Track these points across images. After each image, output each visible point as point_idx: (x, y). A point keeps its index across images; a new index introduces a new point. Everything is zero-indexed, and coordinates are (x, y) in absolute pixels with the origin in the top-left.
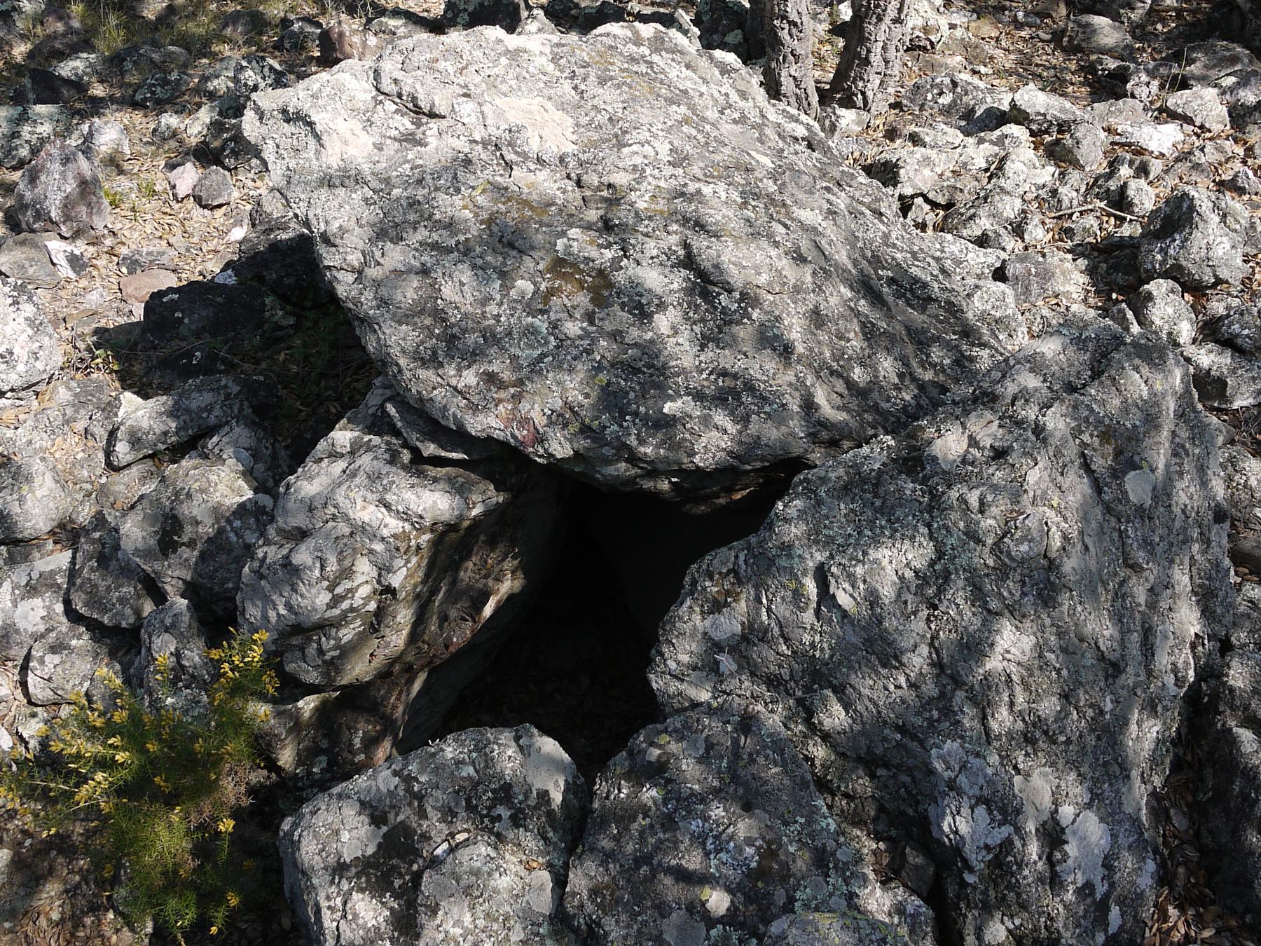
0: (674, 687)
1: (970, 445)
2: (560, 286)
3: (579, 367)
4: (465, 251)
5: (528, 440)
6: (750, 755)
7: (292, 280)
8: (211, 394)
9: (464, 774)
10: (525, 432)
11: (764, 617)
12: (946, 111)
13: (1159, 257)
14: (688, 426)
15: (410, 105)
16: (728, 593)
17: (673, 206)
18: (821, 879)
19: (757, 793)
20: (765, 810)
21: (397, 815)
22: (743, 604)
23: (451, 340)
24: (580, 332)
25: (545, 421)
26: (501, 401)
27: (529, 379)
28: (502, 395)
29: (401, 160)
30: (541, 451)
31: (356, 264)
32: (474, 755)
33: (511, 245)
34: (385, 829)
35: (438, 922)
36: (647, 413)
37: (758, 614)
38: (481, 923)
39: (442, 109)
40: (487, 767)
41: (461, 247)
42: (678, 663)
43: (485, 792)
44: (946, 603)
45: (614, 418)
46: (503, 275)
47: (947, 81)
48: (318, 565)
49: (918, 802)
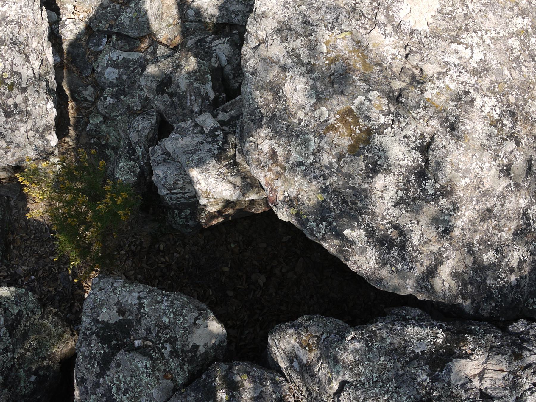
2: (339, 127)
3: (314, 183)
4: (310, 70)
8: (243, 6)
10: (271, 195)
17: (446, 106)
21: (130, 315)
22: (313, 355)
24: (327, 164)
25: (282, 198)
28: (273, 167)
34: (121, 318)
43: (166, 334)
45: (316, 220)
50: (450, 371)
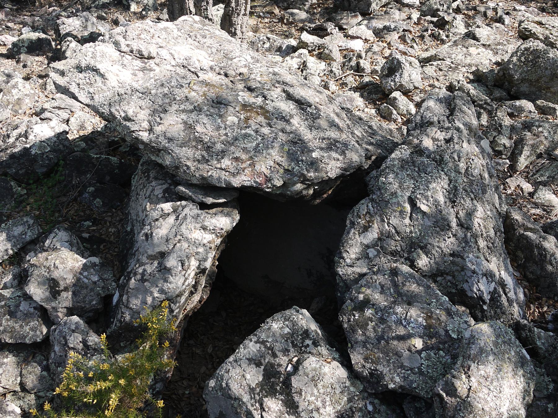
0: (350, 270)
1: (433, 141)
5: (263, 182)
6: (402, 283)
7: (23, 171)
8: (22, 227)
9: (286, 332)
11: (387, 227)
12: (269, 50)
13: (392, 83)
14: (323, 161)
15: (138, 55)
16: (369, 222)
18: (452, 320)
19: (412, 297)
20: (418, 302)
22: (376, 225)
23: (208, 149)
24: (269, 131)
25: (269, 172)
26: (245, 168)
27: (254, 156)
28: (244, 165)
29: (148, 78)
30: (270, 185)
31: (147, 127)
32: (287, 323)
33: (220, 103)
34: (263, 367)
35: (303, 397)
36: (306, 159)
37: (384, 227)
38: (322, 391)
39: (154, 54)
40: (294, 326)
41: (197, 108)
42: (351, 259)
43: (298, 336)
44: (459, 199)
46: (221, 116)
47: (265, 38)
48: (180, 264)
49: (457, 285)
50: (427, 148)
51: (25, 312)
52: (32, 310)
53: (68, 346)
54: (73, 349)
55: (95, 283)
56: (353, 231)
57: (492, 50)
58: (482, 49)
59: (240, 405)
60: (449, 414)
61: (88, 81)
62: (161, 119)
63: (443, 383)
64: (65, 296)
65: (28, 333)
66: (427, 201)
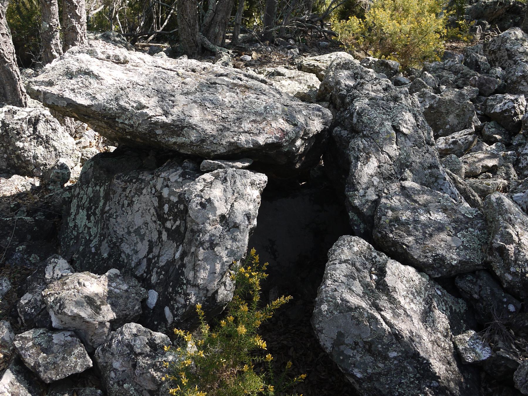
48: (246, 218)
51: (63, 343)
52: (69, 338)
53: (135, 352)
54: (140, 354)
55: (126, 291)
56: (359, 163)
57: (296, 81)
58: (289, 81)
59: (360, 313)
60: (513, 259)
61: (81, 85)
62: (173, 102)
63: (499, 236)
64: (106, 309)
65: (76, 362)
66: (407, 124)
